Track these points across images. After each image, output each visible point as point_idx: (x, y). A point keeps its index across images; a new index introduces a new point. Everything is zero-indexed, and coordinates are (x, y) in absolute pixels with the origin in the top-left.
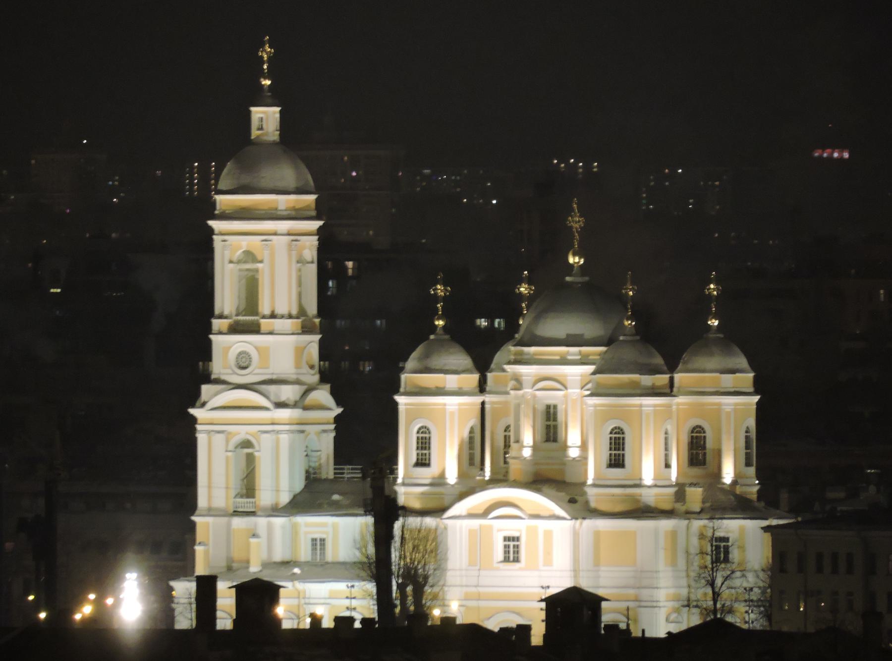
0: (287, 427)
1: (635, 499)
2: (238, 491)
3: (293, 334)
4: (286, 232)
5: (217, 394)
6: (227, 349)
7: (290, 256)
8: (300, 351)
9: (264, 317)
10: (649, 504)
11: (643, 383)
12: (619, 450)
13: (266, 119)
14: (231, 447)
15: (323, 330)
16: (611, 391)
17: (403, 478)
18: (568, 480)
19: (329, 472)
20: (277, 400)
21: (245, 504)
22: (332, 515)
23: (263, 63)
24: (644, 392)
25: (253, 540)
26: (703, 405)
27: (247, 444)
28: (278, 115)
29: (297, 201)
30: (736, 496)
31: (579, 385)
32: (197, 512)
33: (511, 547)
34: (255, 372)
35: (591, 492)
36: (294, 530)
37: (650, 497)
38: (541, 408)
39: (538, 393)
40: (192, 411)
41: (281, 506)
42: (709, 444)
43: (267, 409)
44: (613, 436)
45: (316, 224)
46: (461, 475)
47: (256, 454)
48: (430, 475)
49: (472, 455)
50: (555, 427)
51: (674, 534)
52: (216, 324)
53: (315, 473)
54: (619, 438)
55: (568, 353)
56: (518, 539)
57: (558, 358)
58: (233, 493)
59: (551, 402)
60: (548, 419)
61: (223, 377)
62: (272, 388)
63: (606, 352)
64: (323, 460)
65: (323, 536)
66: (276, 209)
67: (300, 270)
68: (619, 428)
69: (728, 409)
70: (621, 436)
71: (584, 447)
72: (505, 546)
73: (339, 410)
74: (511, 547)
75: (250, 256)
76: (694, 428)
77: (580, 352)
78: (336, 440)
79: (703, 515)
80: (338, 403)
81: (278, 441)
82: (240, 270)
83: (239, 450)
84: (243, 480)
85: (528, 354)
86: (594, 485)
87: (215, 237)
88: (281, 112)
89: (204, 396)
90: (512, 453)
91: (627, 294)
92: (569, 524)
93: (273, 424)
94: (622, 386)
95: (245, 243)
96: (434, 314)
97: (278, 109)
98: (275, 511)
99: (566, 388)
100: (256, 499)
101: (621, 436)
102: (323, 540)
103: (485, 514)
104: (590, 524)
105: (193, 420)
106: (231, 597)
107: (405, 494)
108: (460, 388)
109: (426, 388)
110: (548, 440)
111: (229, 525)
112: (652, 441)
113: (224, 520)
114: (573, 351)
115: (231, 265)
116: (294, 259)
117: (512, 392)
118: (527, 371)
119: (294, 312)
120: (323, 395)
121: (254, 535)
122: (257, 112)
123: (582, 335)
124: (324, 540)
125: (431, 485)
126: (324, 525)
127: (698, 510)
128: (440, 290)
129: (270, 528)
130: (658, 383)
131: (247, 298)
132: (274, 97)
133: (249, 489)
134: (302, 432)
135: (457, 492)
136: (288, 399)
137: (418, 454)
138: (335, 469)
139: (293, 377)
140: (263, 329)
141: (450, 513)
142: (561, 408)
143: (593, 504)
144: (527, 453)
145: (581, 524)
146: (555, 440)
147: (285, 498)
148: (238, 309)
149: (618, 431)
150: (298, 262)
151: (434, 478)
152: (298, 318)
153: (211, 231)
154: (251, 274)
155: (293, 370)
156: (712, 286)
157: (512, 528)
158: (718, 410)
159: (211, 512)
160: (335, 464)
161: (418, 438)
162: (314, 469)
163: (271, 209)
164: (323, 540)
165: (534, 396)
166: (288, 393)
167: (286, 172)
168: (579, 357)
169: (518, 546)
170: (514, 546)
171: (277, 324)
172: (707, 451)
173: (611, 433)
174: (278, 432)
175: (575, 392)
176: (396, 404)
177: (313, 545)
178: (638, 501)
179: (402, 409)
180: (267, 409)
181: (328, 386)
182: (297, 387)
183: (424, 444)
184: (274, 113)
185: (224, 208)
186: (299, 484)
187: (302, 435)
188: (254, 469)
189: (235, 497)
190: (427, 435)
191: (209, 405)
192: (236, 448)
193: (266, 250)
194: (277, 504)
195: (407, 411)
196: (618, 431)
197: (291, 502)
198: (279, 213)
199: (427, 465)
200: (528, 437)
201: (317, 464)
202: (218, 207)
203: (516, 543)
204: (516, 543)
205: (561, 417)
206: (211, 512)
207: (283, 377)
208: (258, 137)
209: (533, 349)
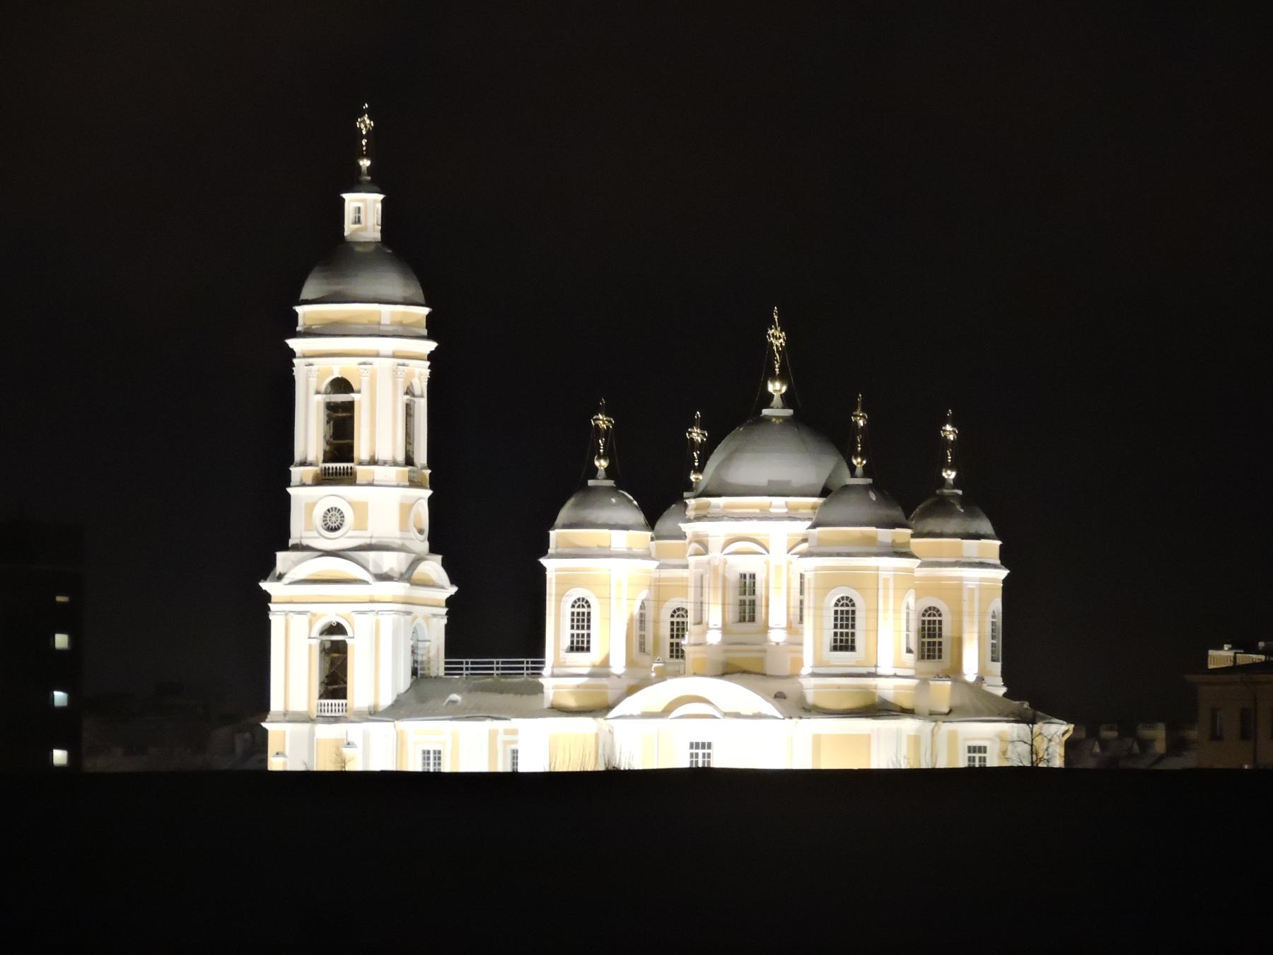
1: (867, 691)
3: (398, 486)
6: (311, 507)
7: (395, 384)
8: (405, 509)
9: (360, 464)
12: (847, 627)
13: (363, 211)
15: (434, 483)
16: (830, 549)
18: (768, 672)
19: (438, 665)
20: (378, 571)
23: (362, 137)
27: (337, 629)
28: (379, 206)
29: (405, 313)
33: (700, 756)
34: (350, 534)
37: (887, 688)
38: (733, 577)
40: (264, 585)
41: (380, 709)
42: (947, 630)
43: (365, 582)
46: (630, 663)
47: (348, 641)
48: (589, 663)
49: (639, 642)
50: (753, 603)
52: (296, 472)
59: (748, 570)
61: (305, 542)
62: (371, 555)
64: (433, 653)
66: (379, 324)
69: (971, 585)
71: (795, 625)
73: (453, 590)
74: (700, 756)
77: (787, 503)
78: (449, 629)
79: (951, 717)
80: (453, 581)
85: (718, 507)
87: (295, 361)
88: (383, 201)
89: (279, 568)
91: (856, 422)
93: (372, 602)
96: (595, 452)
97: (381, 197)
98: (374, 714)
100: (349, 701)
101: (850, 609)
103: (665, 713)
105: (267, 597)
106: (552, 756)
108: (630, 549)
111: (312, 735)
113: (306, 726)
114: (778, 504)
116: (401, 390)
118: (716, 531)
120: (433, 568)
122: (352, 200)
123: (788, 482)
125: (590, 675)
127: (946, 710)
128: (602, 421)
129: (366, 737)
132: (377, 182)
134: (409, 613)
138: (446, 663)
141: (613, 713)
143: (811, 699)
144: (714, 637)
147: (386, 700)
150: (407, 393)
151: (594, 666)
153: (292, 354)
155: (398, 534)
156: (948, 428)
158: (958, 587)
160: (447, 656)
163: (371, 323)
166: (391, 562)
167: (393, 282)
168: (785, 510)
171: (379, 472)
173: (836, 605)
176: (543, 569)
178: (873, 694)
179: (551, 576)
180: (365, 582)
181: (439, 557)
182: (403, 555)
183: (582, 619)
184: (375, 201)
185: (308, 323)
186: (404, 681)
187: (409, 618)
191: (286, 580)
193: (366, 360)
194: (375, 706)
195: (558, 577)
199: (853, 649)
200: (714, 615)
202: (300, 321)
203: (706, 751)
204: (706, 751)
207: (385, 541)
208: (354, 232)
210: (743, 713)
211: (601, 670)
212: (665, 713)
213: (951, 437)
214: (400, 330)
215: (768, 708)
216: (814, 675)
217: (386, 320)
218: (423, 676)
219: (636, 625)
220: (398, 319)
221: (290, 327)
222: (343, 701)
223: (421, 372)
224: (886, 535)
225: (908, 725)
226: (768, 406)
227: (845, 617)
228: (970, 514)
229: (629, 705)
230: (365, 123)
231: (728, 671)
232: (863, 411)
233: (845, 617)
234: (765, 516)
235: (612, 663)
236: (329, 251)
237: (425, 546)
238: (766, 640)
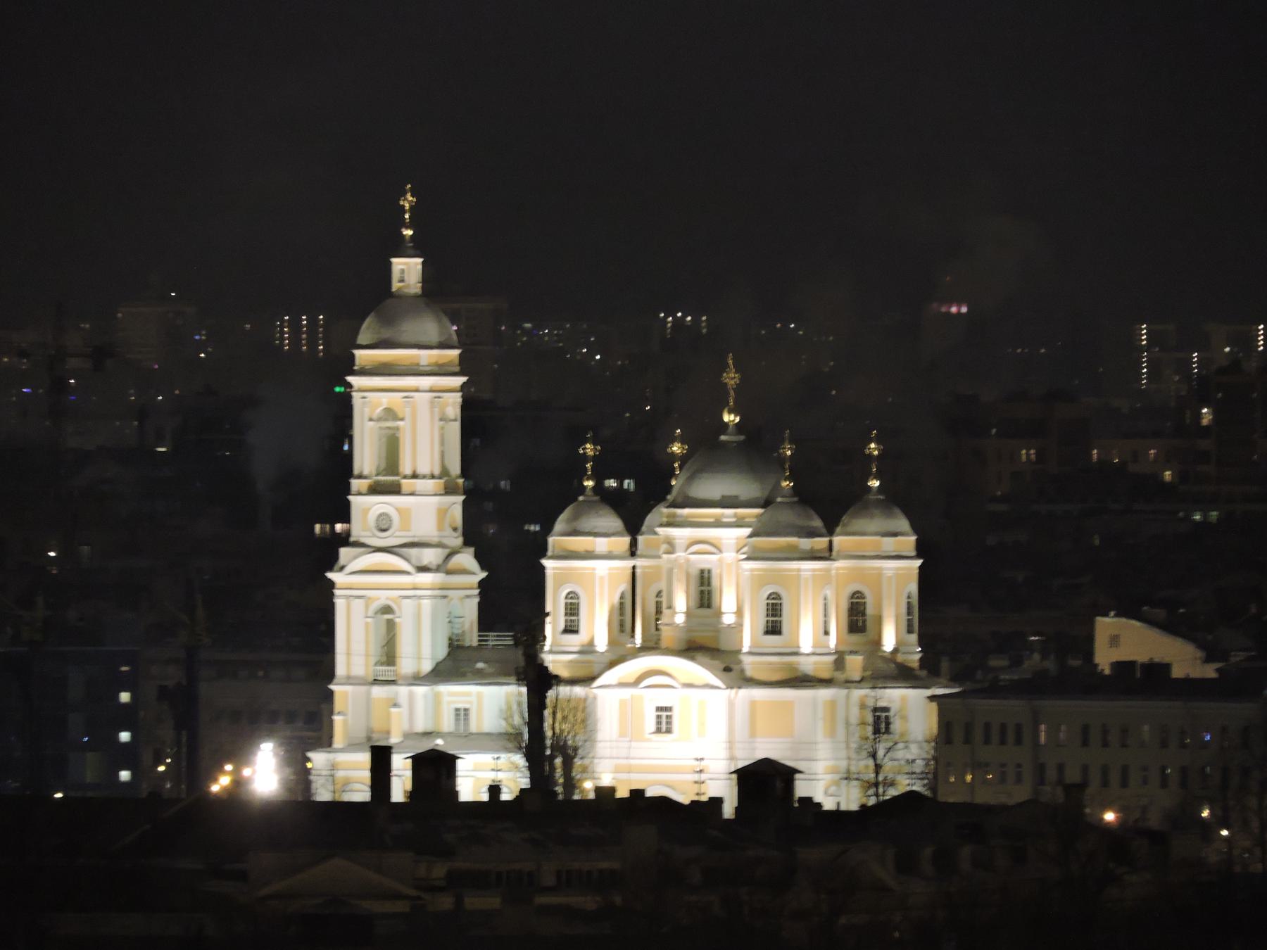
1: (791, 667)
5: (355, 557)
7: (432, 413)
8: (442, 513)
9: (405, 477)
13: (407, 271)
14: (370, 613)
19: (473, 639)
21: (385, 672)
23: (405, 212)
25: (393, 710)
27: (387, 610)
29: (440, 356)
32: (335, 681)
34: (397, 534)
36: (437, 699)
38: (695, 572)
40: (330, 575)
45: (460, 380)
46: (612, 643)
47: (397, 620)
50: (709, 592)
51: (832, 704)
52: (355, 484)
55: (723, 515)
58: (373, 660)
59: (705, 566)
60: (702, 584)
61: (362, 540)
62: (413, 552)
65: (467, 706)
66: (418, 365)
69: (890, 573)
71: (739, 613)
73: (484, 575)
78: (482, 608)
80: (483, 568)
81: (419, 607)
82: (381, 428)
83: (379, 616)
86: (750, 653)
89: (342, 561)
98: (417, 679)
99: (720, 551)
103: (636, 683)
105: (331, 585)
110: (701, 606)
113: (363, 689)
115: (372, 423)
117: (665, 556)
119: (437, 472)
120: (467, 559)
121: (395, 705)
122: (398, 264)
123: (736, 497)
126: (469, 694)
127: (857, 678)
129: (411, 697)
131: (387, 458)
132: (417, 247)
133: (389, 656)
134: (445, 597)
135: (610, 657)
139: (435, 540)
140: (404, 489)
141: (598, 682)
142: (715, 573)
143: (749, 673)
144: (680, 619)
146: (709, 606)
147: (427, 667)
150: (441, 420)
154: (391, 432)
157: (663, 697)
158: (879, 573)
159: (350, 680)
160: (480, 630)
163: (412, 364)
165: (688, 561)
166: (430, 556)
167: (429, 327)
171: (419, 484)
174: (420, 597)
175: (730, 556)
176: (543, 568)
178: (796, 669)
179: (549, 573)
180: (408, 573)
181: (472, 550)
182: (439, 550)
183: (572, 610)
186: (442, 652)
187: (445, 601)
189: (376, 664)
191: (348, 570)
193: (407, 408)
196: (775, 596)
199: (576, 632)
205: (715, 582)
207: (424, 540)
208: (399, 289)
209: (686, 511)
210: (697, 682)
211: (588, 649)
212: (636, 683)
213: (876, 453)
214: (436, 369)
215: (718, 682)
216: (750, 653)
217: (424, 362)
218: (459, 647)
219: (617, 612)
220: (433, 361)
221: (349, 366)
223: (453, 405)
224: (805, 543)
225: (824, 693)
226: (724, 433)
227: (774, 609)
228: (890, 515)
229: (609, 677)
230: (408, 201)
231: (691, 649)
232: (790, 443)
233: (774, 609)
234: (718, 524)
235: (596, 643)
236: (375, 294)
237: (459, 541)
238: (720, 622)
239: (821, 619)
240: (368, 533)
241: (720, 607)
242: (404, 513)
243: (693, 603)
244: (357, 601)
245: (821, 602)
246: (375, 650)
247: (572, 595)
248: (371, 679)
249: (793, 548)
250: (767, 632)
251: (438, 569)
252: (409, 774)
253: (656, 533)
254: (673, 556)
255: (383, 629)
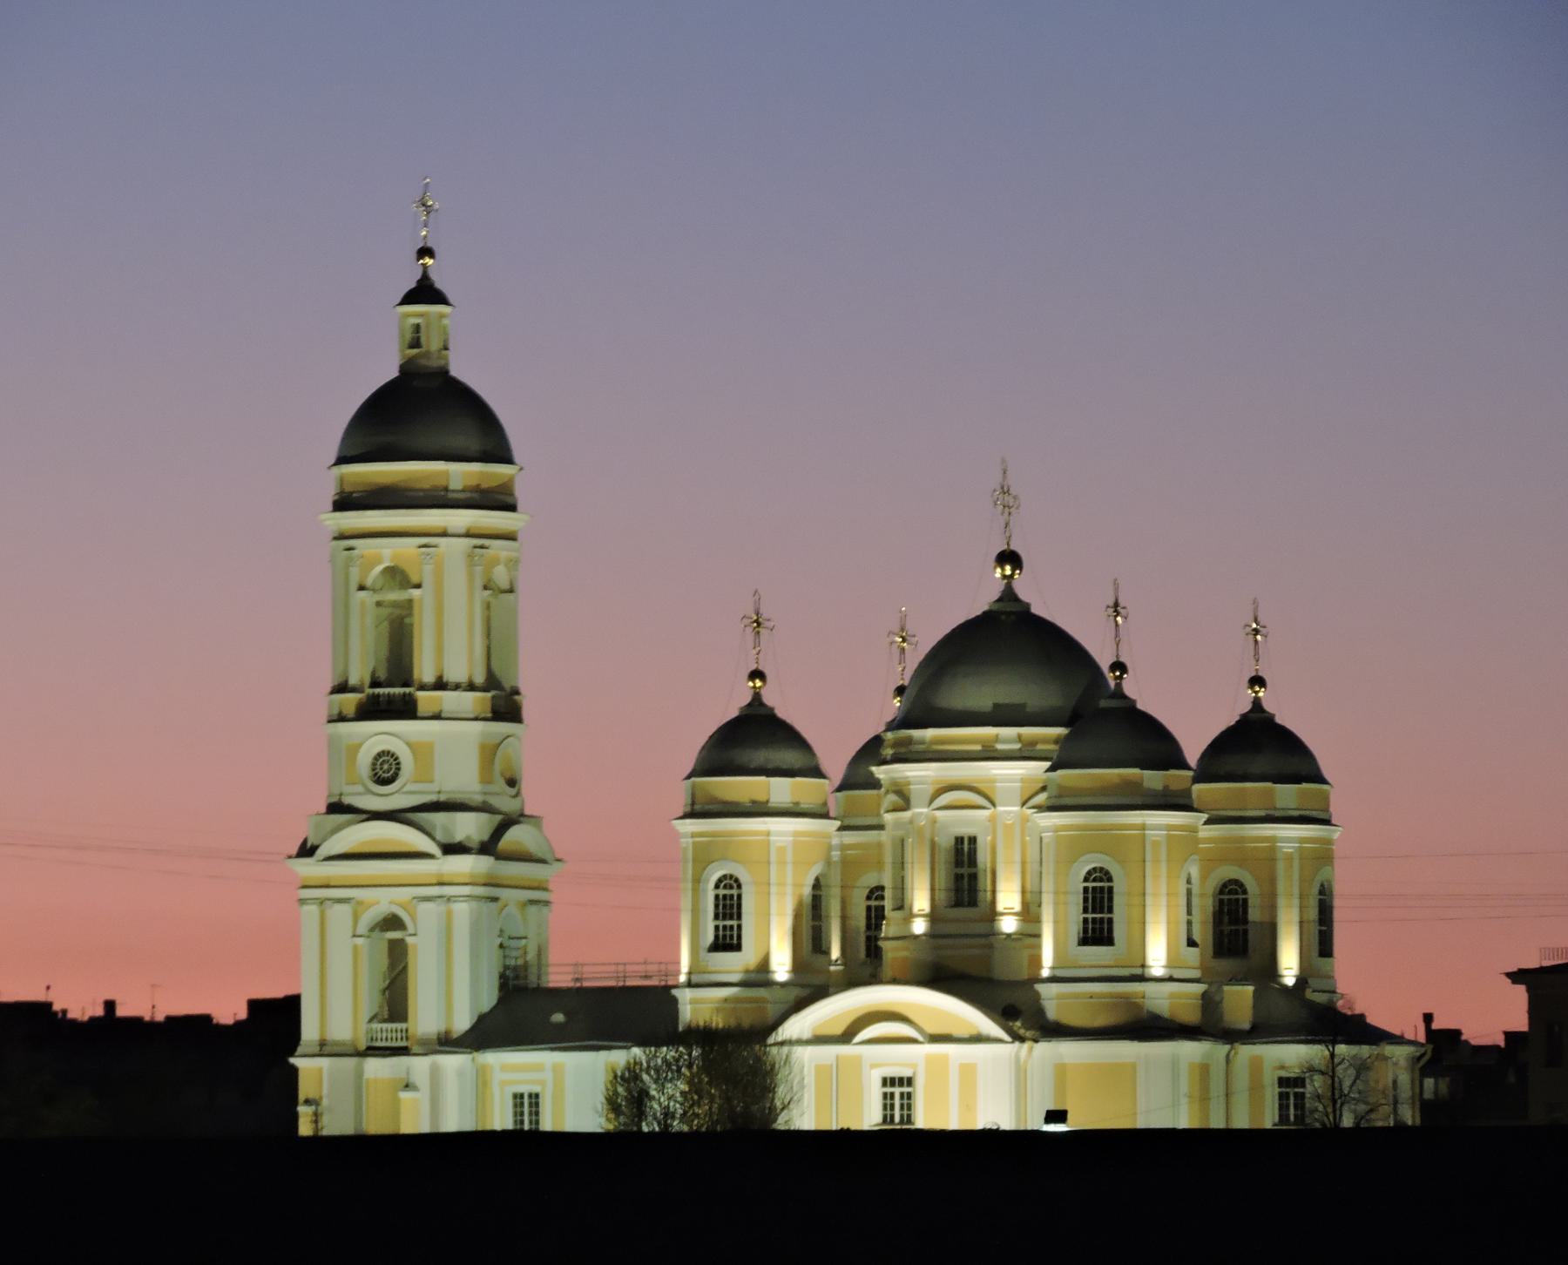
0: (466, 890)
1: (1128, 1002)
2: (376, 1009)
3: (476, 719)
4: (463, 531)
5: (339, 828)
9: (423, 687)
10: (1157, 1011)
11: (1146, 784)
12: (731, 918)
14: (362, 928)
17: (690, 973)
21: (387, 1032)
22: (553, 1049)
24: (1148, 801)
25: (405, 1096)
26: (1242, 839)
27: (393, 922)
30: (1312, 1005)
31: (1019, 801)
32: (300, 1050)
33: (897, 1097)
34: (409, 788)
35: (1048, 992)
36: (481, 1080)
38: (946, 842)
39: (939, 814)
41: (455, 1036)
42: (1254, 914)
44: (1090, 885)
46: (798, 966)
47: (409, 940)
49: (810, 939)
50: (974, 877)
51: (1204, 1070)
53: (517, 977)
54: (1102, 888)
55: (997, 739)
56: (910, 1081)
57: (978, 748)
58: (365, 1015)
59: (966, 831)
60: (958, 863)
62: (439, 818)
63: (1067, 737)
65: (535, 1089)
66: (446, 489)
67: (488, 606)
68: (1101, 869)
69: (1288, 848)
70: (1106, 884)
71: (1030, 913)
72: (885, 1095)
74: (897, 1097)
75: (397, 576)
76: (1225, 885)
81: (449, 915)
82: (379, 604)
83: (376, 934)
84: (384, 991)
86: (1053, 979)
90: (887, 929)
92: (1009, 1050)
94: (1105, 790)
95: (388, 552)
98: (447, 1043)
99: (994, 805)
101: (1106, 884)
102: (535, 1097)
103: (846, 1037)
104: (1048, 1051)
107: (693, 1002)
108: (797, 804)
109: (736, 804)
110: (958, 903)
111: (359, 1074)
112: (1163, 901)
113: (352, 1061)
115: (362, 594)
116: (479, 583)
117: (888, 818)
119: (479, 679)
121: (407, 1086)
123: (1024, 706)
124: (537, 1096)
125: (743, 984)
126: (539, 1068)
130: (1174, 786)
131: (389, 660)
133: (395, 1003)
134: (495, 899)
135: (794, 993)
136: (468, 837)
137: (717, 928)
139: (478, 799)
140: (422, 708)
143: (1052, 1012)
144: (919, 927)
145: (1031, 1049)
146: (973, 903)
147: (462, 1022)
148: (373, 673)
149: (1100, 875)
150: (485, 588)
151: (747, 971)
152: (485, 689)
154: (398, 612)
155: (477, 787)
157: (899, 1059)
158: (1268, 858)
159: (325, 1049)
161: (717, 897)
162: (515, 968)
163: (435, 489)
164: (535, 1097)
165: (934, 821)
166: (469, 827)
168: (1018, 746)
169: (909, 1095)
170: (902, 1095)
171: (449, 700)
172: (1249, 927)
173: (1086, 880)
174: (449, 899)
175: (1009, 810)
177: (515, 1106)
178: (1138, 1007)
182: (484, 816)
186: (488, 998)
187: (493, 905)
188: (405, 969)
189: (371, 1021)
190: (735, 892)
191: (322, 852)
192: (372, 930)
194: (447, 1033)
196: (1100, 875)
197: (474, 1028)
198: (451, 495)
199: (737, 947)
201: (520, 962)
203: (906, 1089)
204: (906, 1089)
205: (983, 857)
206: (325, 1049)
207: (458, 797)
209: (930, 733)
210: (956, 1033)
216: (1053, 979)
217: (455, 484)
220: (473, 482)
222: (404, 1026)
229: (798, 1025)
231: (939, 977)
234: (989, 754)
239: (1183, 917)
240: (360, 788)
241: (993, 902)
242: (421, 751)
243: (942, 896)
244: (338, 907)
245: (1182, 888)
246: (370, 1001)
247: (730, 882)
248: (362, 1046)
249: (1132, 786)
250: (1085, 941)
251: (487, 848)
252: (414, 1119)
253: (875, 784)
254: (907, 815)
255: (384, 961)
